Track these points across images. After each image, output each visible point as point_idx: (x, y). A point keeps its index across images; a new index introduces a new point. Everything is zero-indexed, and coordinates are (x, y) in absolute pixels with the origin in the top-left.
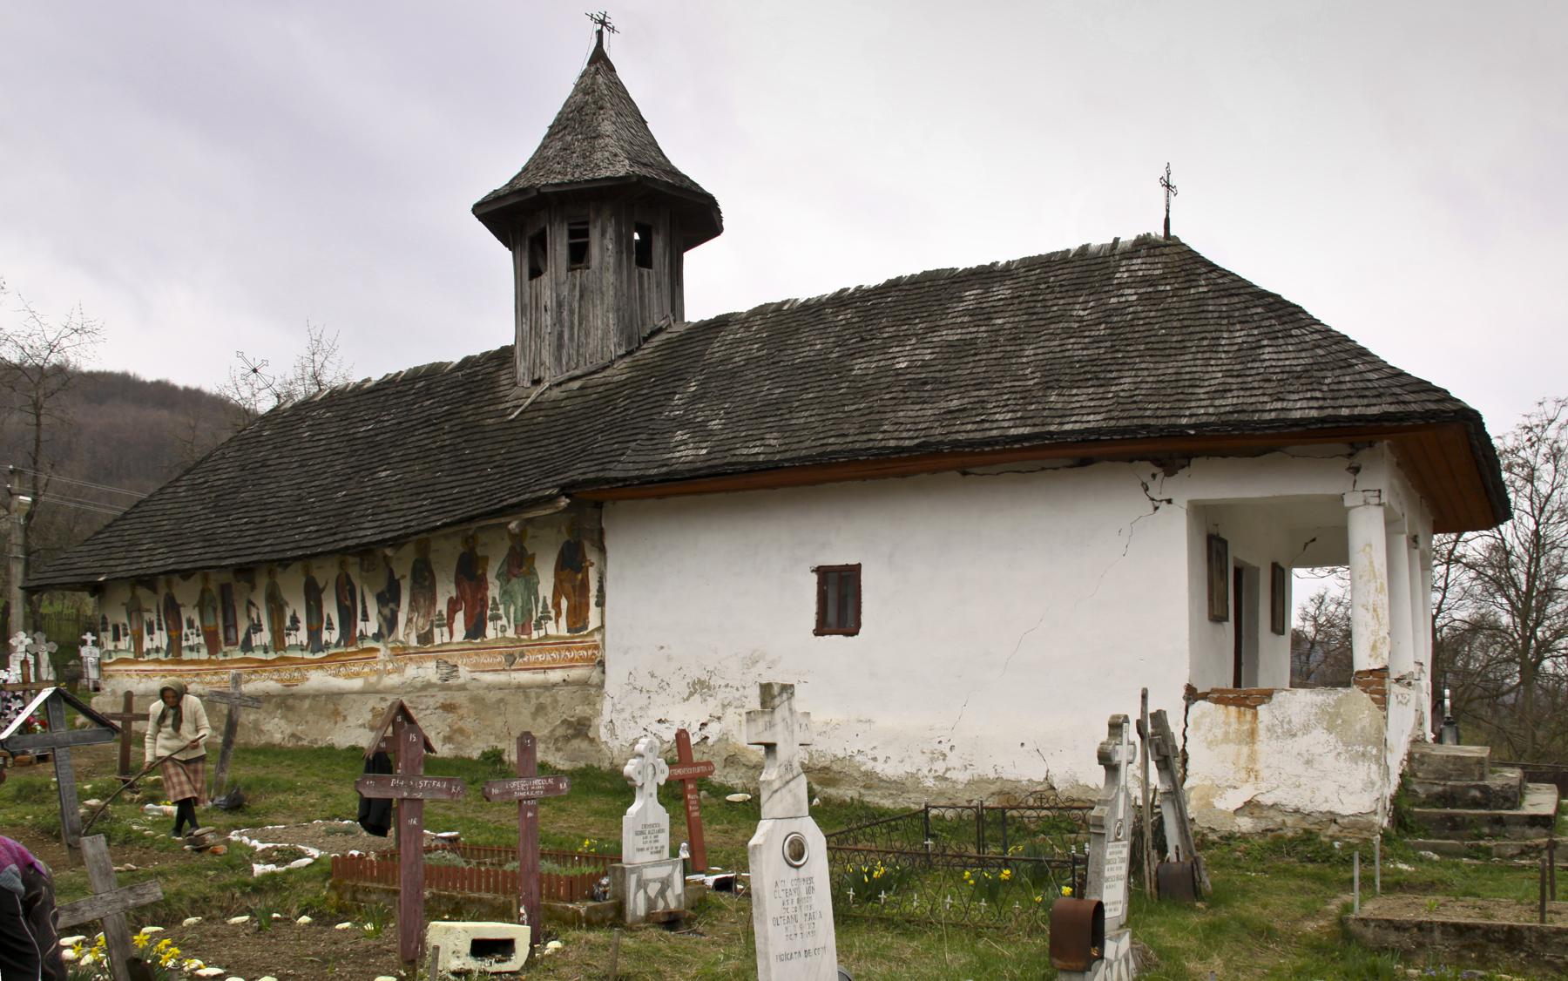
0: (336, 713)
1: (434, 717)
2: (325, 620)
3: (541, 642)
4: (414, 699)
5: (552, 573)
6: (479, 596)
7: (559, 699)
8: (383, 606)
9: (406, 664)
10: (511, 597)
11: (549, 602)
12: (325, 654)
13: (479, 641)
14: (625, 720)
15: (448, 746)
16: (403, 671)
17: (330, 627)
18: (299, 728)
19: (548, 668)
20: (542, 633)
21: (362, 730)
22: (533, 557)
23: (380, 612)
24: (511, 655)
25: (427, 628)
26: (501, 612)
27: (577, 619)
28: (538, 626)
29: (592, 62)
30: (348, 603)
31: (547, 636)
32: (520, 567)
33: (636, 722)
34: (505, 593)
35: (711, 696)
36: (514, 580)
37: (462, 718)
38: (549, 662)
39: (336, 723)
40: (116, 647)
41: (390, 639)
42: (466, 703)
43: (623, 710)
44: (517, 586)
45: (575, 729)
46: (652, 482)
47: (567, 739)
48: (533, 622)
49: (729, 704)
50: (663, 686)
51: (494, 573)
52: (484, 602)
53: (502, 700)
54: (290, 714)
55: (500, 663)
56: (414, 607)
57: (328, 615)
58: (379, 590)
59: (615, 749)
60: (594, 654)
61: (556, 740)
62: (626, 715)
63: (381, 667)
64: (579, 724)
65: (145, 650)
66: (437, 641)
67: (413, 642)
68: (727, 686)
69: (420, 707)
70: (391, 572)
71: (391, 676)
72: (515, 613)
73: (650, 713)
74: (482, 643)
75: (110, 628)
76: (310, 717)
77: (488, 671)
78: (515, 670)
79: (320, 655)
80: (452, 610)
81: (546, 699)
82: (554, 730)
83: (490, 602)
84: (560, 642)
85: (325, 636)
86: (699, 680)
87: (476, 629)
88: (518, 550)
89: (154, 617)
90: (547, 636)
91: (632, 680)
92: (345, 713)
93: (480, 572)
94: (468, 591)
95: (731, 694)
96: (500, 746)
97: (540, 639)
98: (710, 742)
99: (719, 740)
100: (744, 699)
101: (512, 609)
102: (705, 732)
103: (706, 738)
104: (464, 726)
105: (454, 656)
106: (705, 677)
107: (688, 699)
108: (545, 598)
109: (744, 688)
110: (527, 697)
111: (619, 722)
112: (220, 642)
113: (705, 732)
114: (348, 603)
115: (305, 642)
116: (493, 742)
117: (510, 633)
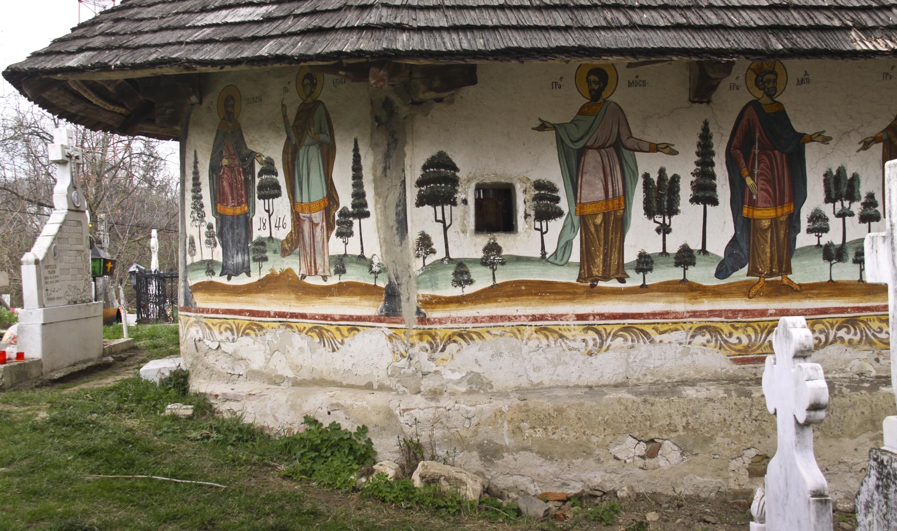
40: (492, 248)
75: (467, 193)
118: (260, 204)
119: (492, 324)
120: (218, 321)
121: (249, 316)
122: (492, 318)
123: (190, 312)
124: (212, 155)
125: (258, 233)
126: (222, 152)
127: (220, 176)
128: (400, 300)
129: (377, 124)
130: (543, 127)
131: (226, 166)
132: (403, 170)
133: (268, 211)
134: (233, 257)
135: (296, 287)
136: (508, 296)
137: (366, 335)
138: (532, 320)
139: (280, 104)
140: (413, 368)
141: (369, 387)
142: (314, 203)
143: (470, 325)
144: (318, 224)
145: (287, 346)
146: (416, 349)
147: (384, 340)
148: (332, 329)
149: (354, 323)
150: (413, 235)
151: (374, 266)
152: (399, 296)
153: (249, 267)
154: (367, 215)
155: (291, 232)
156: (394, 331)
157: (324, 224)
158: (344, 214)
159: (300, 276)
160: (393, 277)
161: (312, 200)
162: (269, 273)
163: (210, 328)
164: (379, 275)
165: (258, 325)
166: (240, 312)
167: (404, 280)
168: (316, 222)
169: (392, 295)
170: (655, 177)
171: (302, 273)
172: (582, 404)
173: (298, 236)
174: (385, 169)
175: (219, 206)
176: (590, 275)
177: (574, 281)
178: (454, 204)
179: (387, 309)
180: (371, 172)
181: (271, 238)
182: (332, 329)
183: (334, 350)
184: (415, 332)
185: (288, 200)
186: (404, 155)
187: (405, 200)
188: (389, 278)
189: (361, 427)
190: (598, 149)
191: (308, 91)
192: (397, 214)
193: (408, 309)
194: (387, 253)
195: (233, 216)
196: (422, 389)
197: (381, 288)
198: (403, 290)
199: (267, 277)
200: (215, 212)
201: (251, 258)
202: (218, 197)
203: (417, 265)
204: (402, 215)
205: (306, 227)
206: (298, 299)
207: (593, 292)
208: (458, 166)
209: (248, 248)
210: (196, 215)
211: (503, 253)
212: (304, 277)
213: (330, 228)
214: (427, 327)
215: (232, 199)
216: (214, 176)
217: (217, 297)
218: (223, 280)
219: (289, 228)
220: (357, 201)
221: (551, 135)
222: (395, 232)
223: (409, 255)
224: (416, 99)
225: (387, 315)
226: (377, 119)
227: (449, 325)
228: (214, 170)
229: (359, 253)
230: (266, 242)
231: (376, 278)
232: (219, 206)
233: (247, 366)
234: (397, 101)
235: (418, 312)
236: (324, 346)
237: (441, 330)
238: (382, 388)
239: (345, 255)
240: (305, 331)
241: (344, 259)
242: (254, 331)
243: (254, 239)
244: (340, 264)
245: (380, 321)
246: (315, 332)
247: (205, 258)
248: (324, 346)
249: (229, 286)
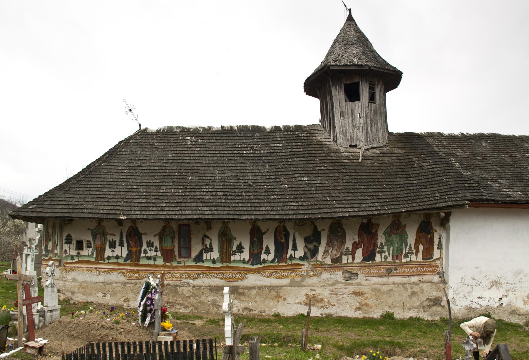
0: (278, 297)
1: (348, 299)
2: (264, 248)
3: (407, 263)
4: (334, 290)
5: (415, 234)
6: (373, 242)
7: (424, 289)
8: (308, 243)
9: (321, 273)
10: (391, 243)
11: (413, 246)
12: (262, 266)
13: (370, 262)
14: (461, 297)
15: (358, 312)
16: (320, 275)
17: (268, 251)
18: (250, 304)
19: (411, 275)
20: (408, 260)
21: (299, 305)
22: (405, 226)
23: (306, 246)
24: (390, 269)
25: (338, 256)
26: (385, 249)
27: (428, 254)
28: (406, 256)
29: (347, 20)
30: (283, 241)
31: (410, 261)
32: (397, 230)
33: (467, 298)
34: (387, 241)
35: (501, 287)
36: (393, 236)
37: (367, 298)
38: (411, 272)
39: (278, 302)
40: (78, 253)
41: (312, 260)
42: (370, 292)
43: (459, 293)
44: (395, 238)
45: (434, 302)
46: (507, 203)
47: (429, 306)
48: (403, 255)
49: (509, 290)
50: (479, 283)
51: (383, 232)
52: (375, 245)
53: (391, 290)
54: (242, 297)
55: (383, 273)
56: (329, 244)
57: (267, 247)
58: (306, 235)
59: (456, 310)
60: (436, 269)
61: (424, 307)
62: (461, 295)
63: (305, 273)
64: (435, 300)
65: (106, 256)
66: (344, 261)
67: (328, 261)
68: (507, 283)
69: (339, 294)
70: (316, 227)
71: (311, 278)
72: (393, 250)
73: (473, 294)
74: (373, 263)
75: (74, 242)
76: (258, 299)
77: (376, 276)
78: (391, 276)
79: (259, 266)
80: (356, 246)
81: (416, 289)
82: (422, 303)
83: (379, 245)
84: (418, 264)
85: (263, 256)
86: (495, 281)
87: (369, 256)
88: (397, 222)
89: (117, 239)
90: (410, 261)
91: (463, 280)
92: (285, 297)
93: (374, 231)
94: (366, 239)
95: (509, 286)
96: (391, 311)
97: (406, 262)
98: (504, 305)
99: (507, 305)
100: (515, 288)
101: (391, 249)
102: (501, 302)
103: (502, 304)
104: (368, 302)
105: (355, 269)
106: (497, 279)
107: (490, 288)
108: (410, 244)
109: (515, 284)
110: (405, 288)
111: (458, 298)
112: (175, 256)
113: (501, 302)
114: (283, 241)
115: (247, 259)
116: (387, 309)
117: (390, 259)
122: (78, 267)
130: (89, 229)
150: (64, 250)
169: (60, 261)
193: (62, 264)
198: (62, 260)
239: (156, 256)
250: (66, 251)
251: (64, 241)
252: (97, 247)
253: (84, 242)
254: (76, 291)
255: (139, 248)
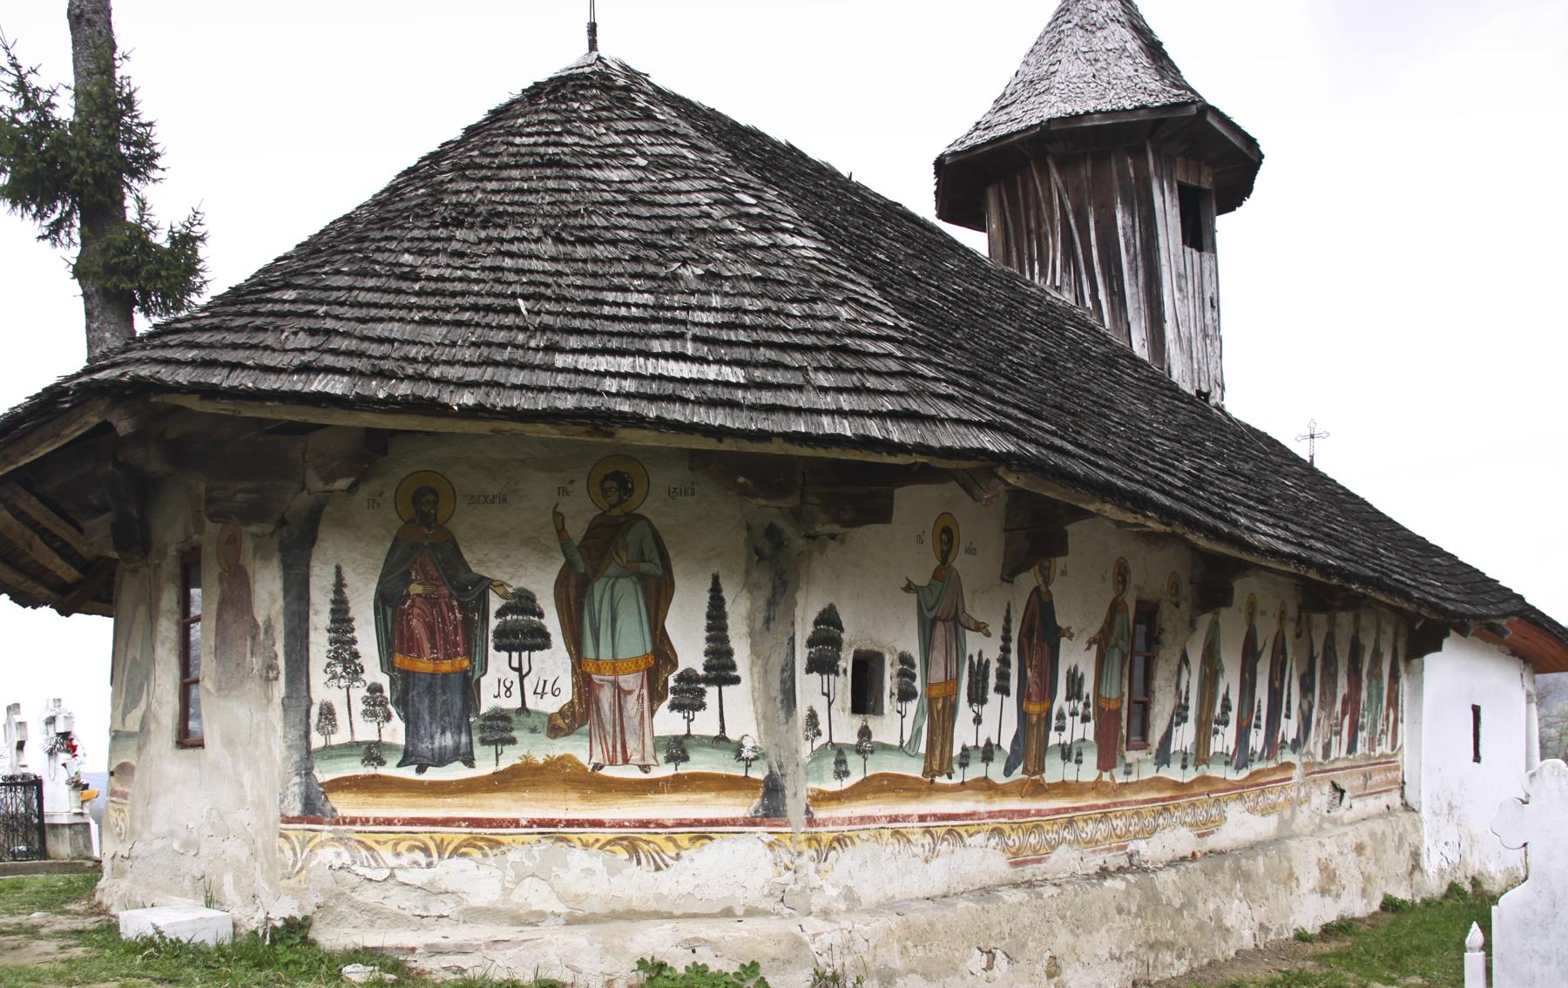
40: (865, 733)
75: (846, 662)
118: (498, 663)
119: (861, 827)
120: (392, 836)
121: (467, 826)
122: (862, 819)
123: (321, 823)
124: (382, 577)
125: (488, 701)
126: (408, 573)
127: (403, 612)
128: (784, 795)
129: (756, 558)
130: (909, 588)
131: (419, 595)
132: (793, 624)
133: (519, 670)
134: (432, 737)
135: (581, 782)
136: (875, 792)
137: (725, 844)
138: (890, 822)
139: (551, 511)
140: (801, 884)
141: (728, 913)
142: (624, 661)
143: (845, 828)
144: (630, 692)
145: (555, 869)
146: (805, 858)
147: (761, 849)
148: (659, 839)
149: (703, 831)
150: (802, 712)
151: (745, 750)
152: (783, 790)
153: (471, 753)
154: (737, 680)
155: (572, 701)
156: (776, 836)
157: (645, 691)
158: (688, 678)
159: (590, 767)
160: (775, 765)
161: (620, 656)
162: (518, 761)
163: (369, 848)
164: (754, 763)
165: (488, 840)
166: (447, 822)
167: (790, 769)
168: (626, 688)
169: (773, 790)
170: (975, 659)
171: (594, 760)
172: (945, 916)
173: (588, 709)
174: (768, 620)
175: (398, 658)
176: (931, 770)
177: (920, 776)
178: (837, 674)
179: (766, 808)
180: (745, 622)
181: (524, 709)
182: (659, 839)
183: (658, 868)
184: (803, 837)
185: (567, 655)
186: (795, 604)
187: (794, 663)
188: (770, 767)
189: (748, 964)
190: (944, 621)
191: (614, 498)
192: (783, 682)
193: (795, 806)
194: (766, 732)
195: (433, 675)
196: (813, 909)
197: (756, 781)
198: (788, 784)
199: (514, 768)
200: (387, 664)
201: (475, 739)
202: (393, 642)
203: (806, 750)
204: (789, 684)
205: (606, 697)
206: (585, 798)
207: (932, 789)
208: (844, 625)
209: (469, 725)
210: (339, 670)
211: (873, 739)
212: (598, 767)
213: (656, 696)
214: (814, 830)
215: (432, 648)
216: (389, 612)
217: (388, 799)
218: (409, 773)
219: (567, 695)
220: (715, 661)
221: (913, 597)
222: (779, 706)
223: (797, 736)
224: (811, 532)
225: (766, 816)
226: (757, 551)
227: (831, 828)
228: (385, 601)
229: (716, 732)
230: (513, 716)
231: (747, 767)
232: (398, 658)
233: (460, 901)
234: (789, 531)
235: (808, 812)
236: (639, 863)
237: (825, 833)
238: (751, 912)
239: (688, 735)
240: (598, 845)
241: (686, 742)
242: (481, 848)
243: (484, 709)
244: (677, 748)
245: (755, 824)
246: (621, 845)
247: (359, 737)
248: (639, 863)
249: (421, 783)
250: (328, 712)
251: (802, 656)
252: (934, 693)
253: (888, 659)
254: (898, 964)
255: (1046, 705)
